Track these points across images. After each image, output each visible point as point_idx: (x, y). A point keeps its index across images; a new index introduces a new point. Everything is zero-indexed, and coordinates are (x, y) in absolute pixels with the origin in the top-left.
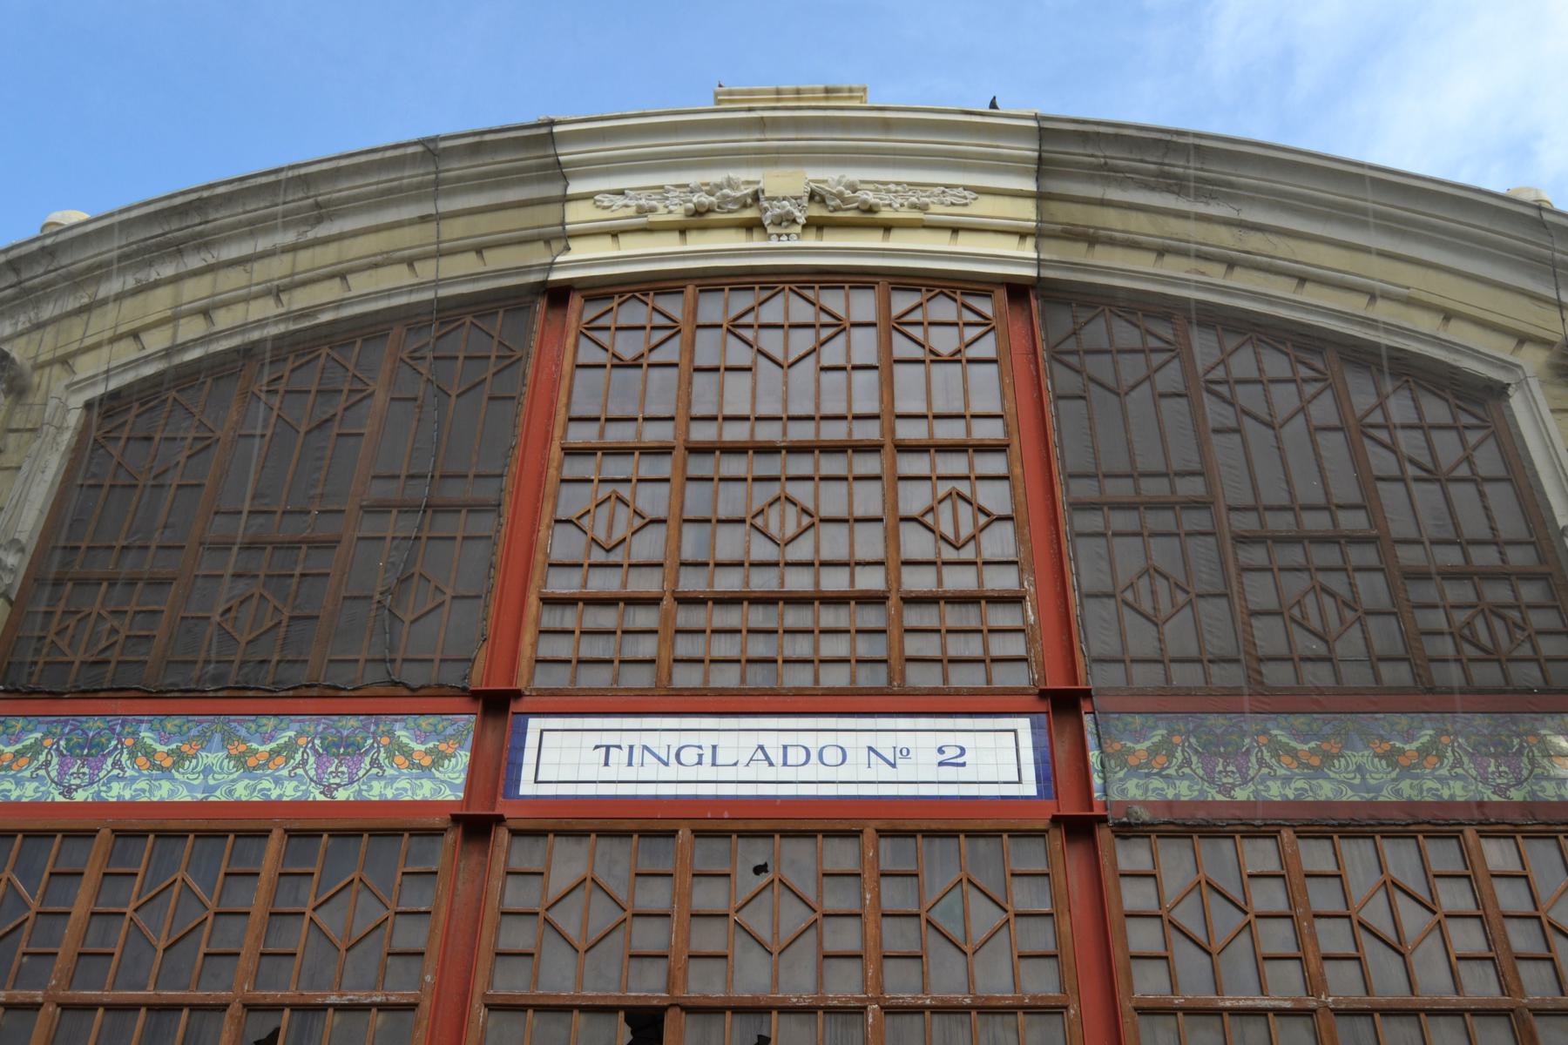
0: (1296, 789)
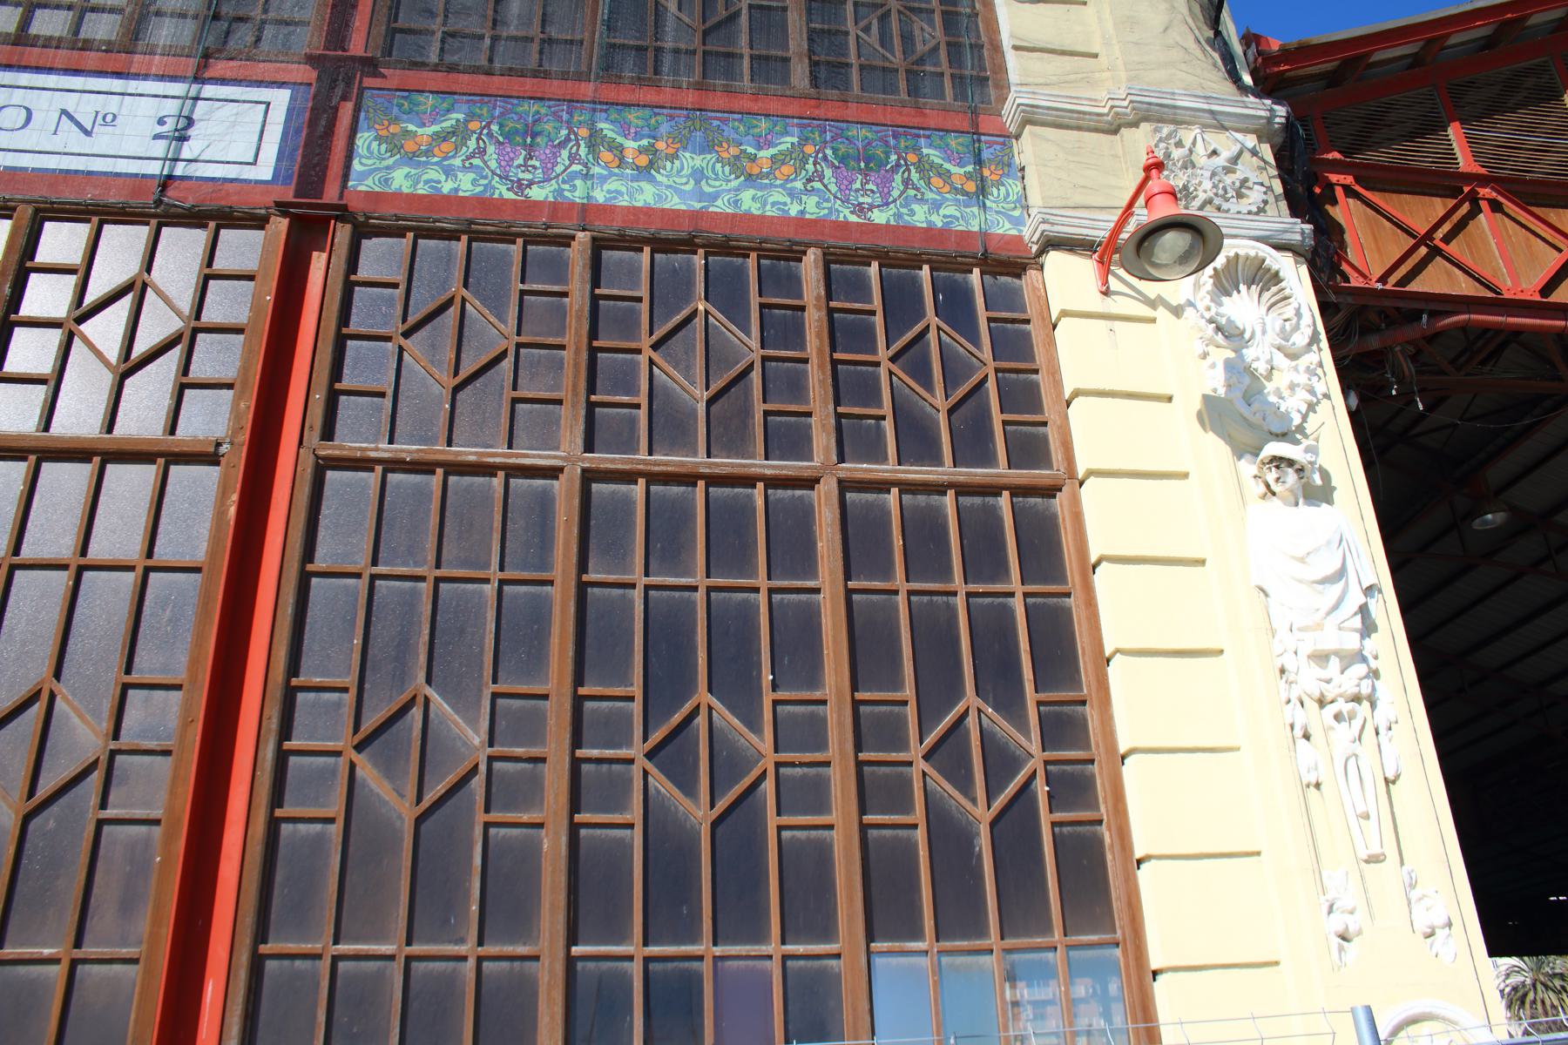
0: (944, 216)
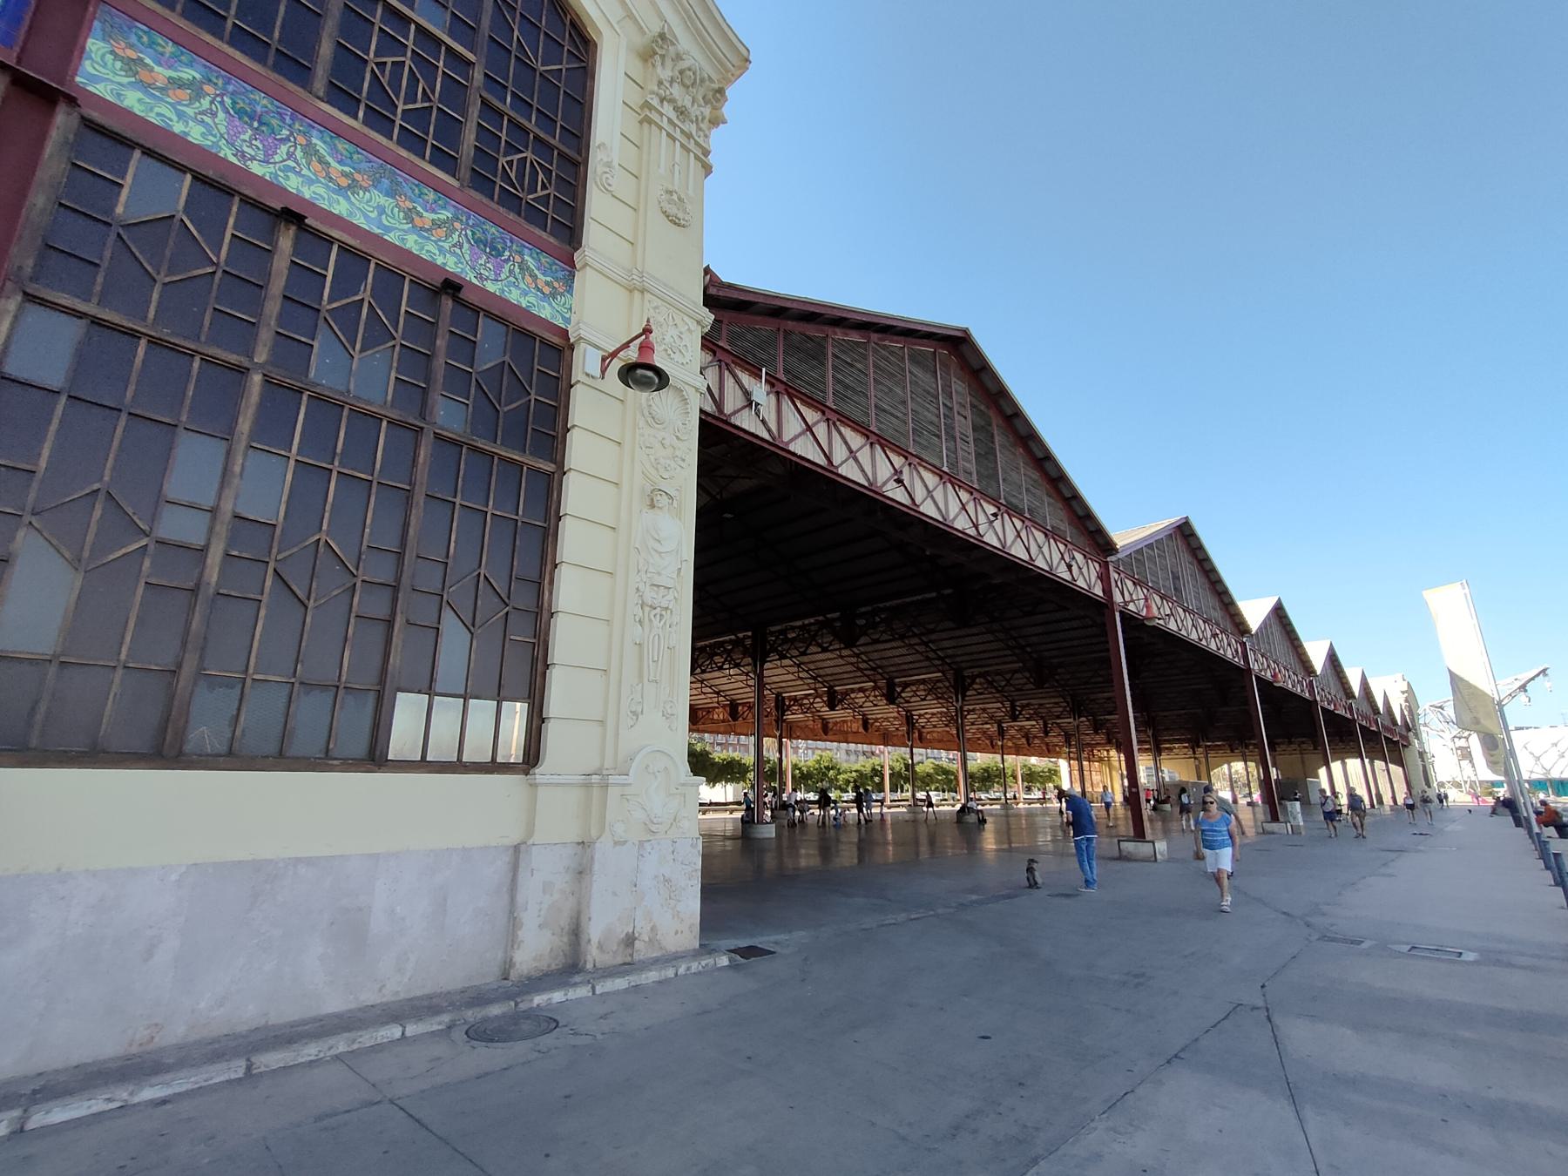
0: (314, 193)
